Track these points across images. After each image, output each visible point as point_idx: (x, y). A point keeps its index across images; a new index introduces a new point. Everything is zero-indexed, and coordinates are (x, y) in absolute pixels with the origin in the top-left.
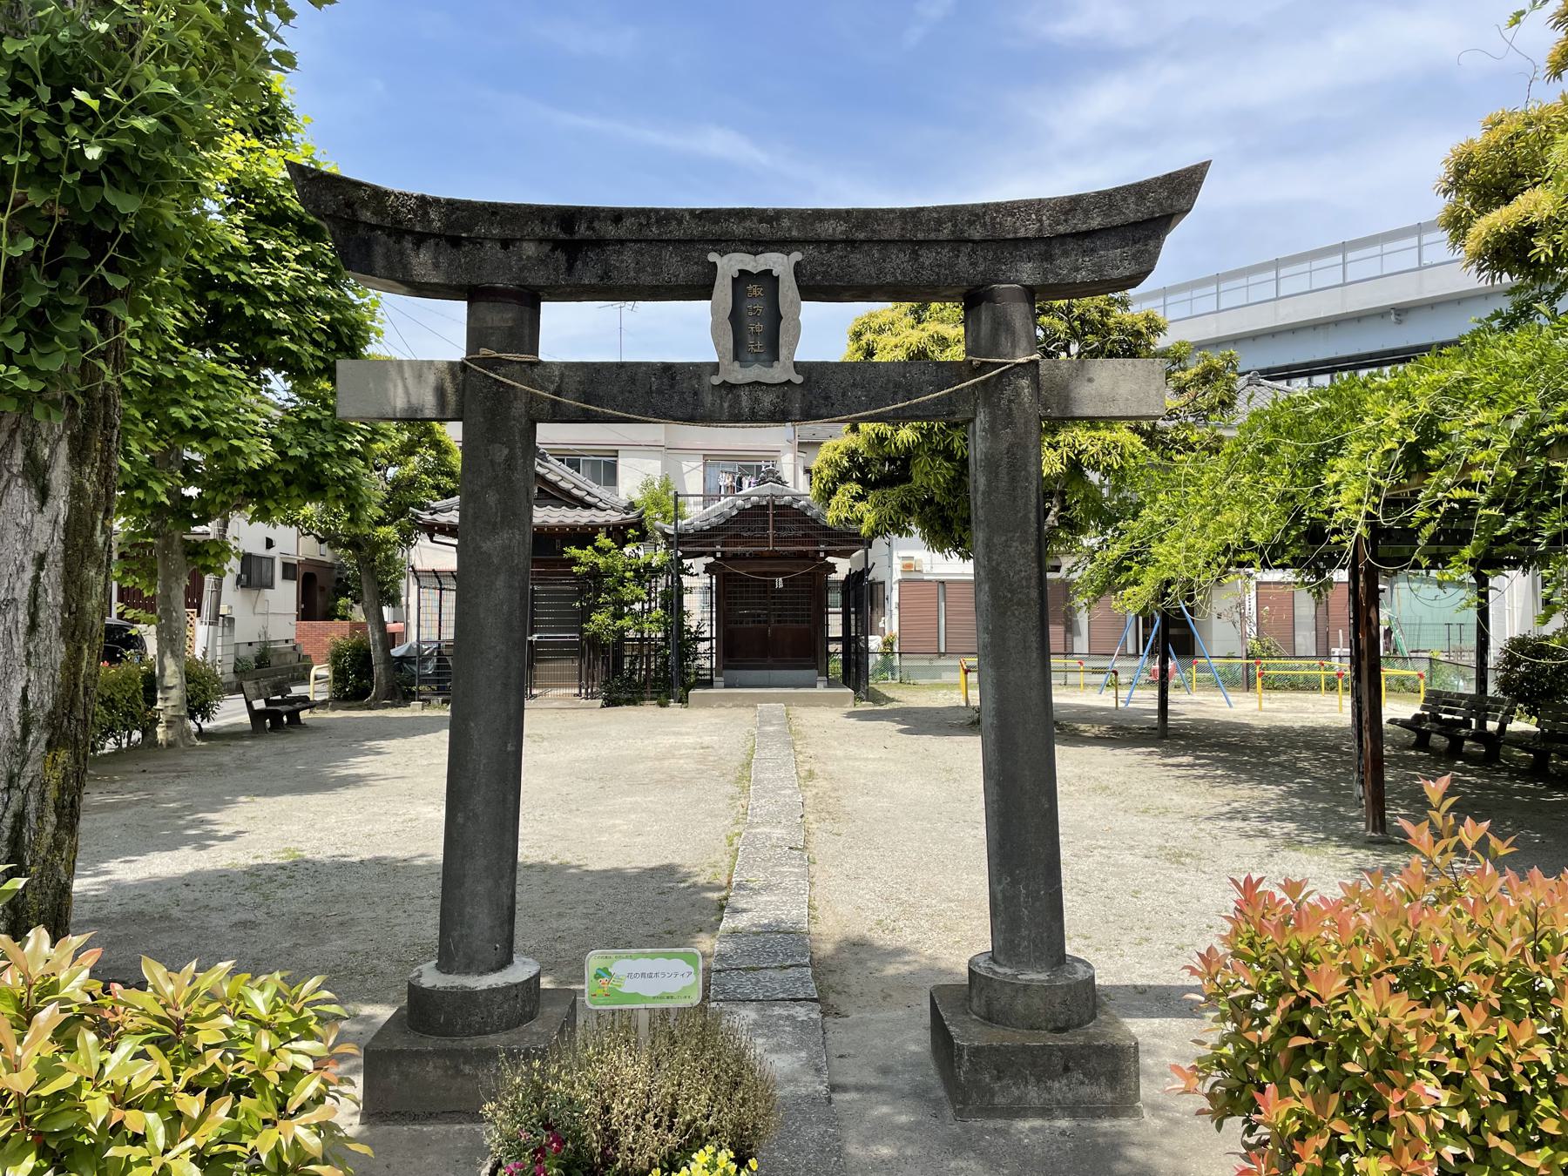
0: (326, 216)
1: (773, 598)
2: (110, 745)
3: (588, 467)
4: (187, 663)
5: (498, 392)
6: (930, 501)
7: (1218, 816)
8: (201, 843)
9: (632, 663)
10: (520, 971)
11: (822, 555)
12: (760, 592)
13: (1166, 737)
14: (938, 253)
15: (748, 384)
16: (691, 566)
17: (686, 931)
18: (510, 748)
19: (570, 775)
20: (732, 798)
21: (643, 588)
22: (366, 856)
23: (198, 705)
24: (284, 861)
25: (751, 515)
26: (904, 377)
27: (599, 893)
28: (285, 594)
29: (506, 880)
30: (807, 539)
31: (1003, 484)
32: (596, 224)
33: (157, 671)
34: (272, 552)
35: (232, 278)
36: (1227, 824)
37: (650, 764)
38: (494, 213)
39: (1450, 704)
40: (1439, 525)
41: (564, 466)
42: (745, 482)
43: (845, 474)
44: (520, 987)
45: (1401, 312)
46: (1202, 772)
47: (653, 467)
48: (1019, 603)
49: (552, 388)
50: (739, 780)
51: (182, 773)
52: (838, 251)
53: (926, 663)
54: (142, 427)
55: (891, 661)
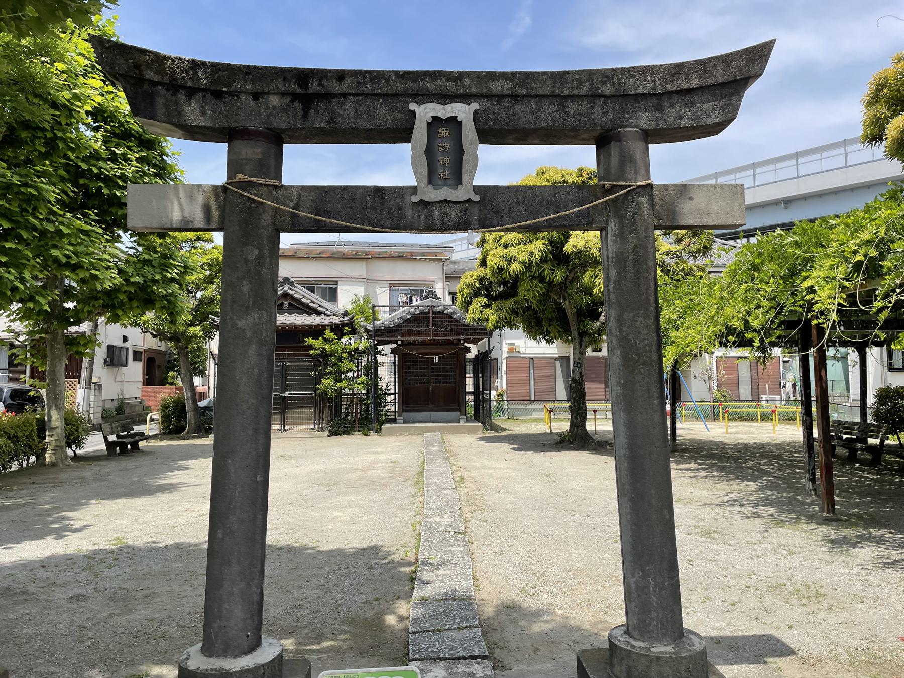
0: (121, 75)
1: (433, 368)
2: (15, 466)
3: (320, 291)
4: (66, 413)
5: (251, 207)
6: (529, 308)
7: (723, 504)
8: (59, 534)
9: (346, 409)
10: (267, 653)
11: (462, 342)
12: (424, 365)
13: (675, 451)
14: (579, 105)
15: (439, 202)
16: (383, 350)
17: (389, 598)
18: (259, 478)
19: (308, 481)
20: (413, 496)
21: (353, 363)
22: (170, 542)
23: (74, 439)
24: (113, 547)
25: (418, 318)
26: (554, 196)
27: (327, 568)
28: (135, 370)
29: (256, 581)
30: (452, 332)
31: (630, 275)
32: (325, 82)
33: (46, 418)
34: (127, 344)
35: (95, 170)
36: (732, 509)
37: (359, 473)
38: (247, 74)
39: (848, 428)
40: (891, 311)
41: (305, 290)
42: (414, 299)
43: (477, 292)
44: (266, 667)
45: (787, 202)
46: (704, 473)
47: (359, 291)
48: (644, 364)
49: (292, 205)
50: (416, 484)
51: (57, 484)
52: (506, 103)
53: (523, 407)
54: (32, 262)
55: (502, 405)
